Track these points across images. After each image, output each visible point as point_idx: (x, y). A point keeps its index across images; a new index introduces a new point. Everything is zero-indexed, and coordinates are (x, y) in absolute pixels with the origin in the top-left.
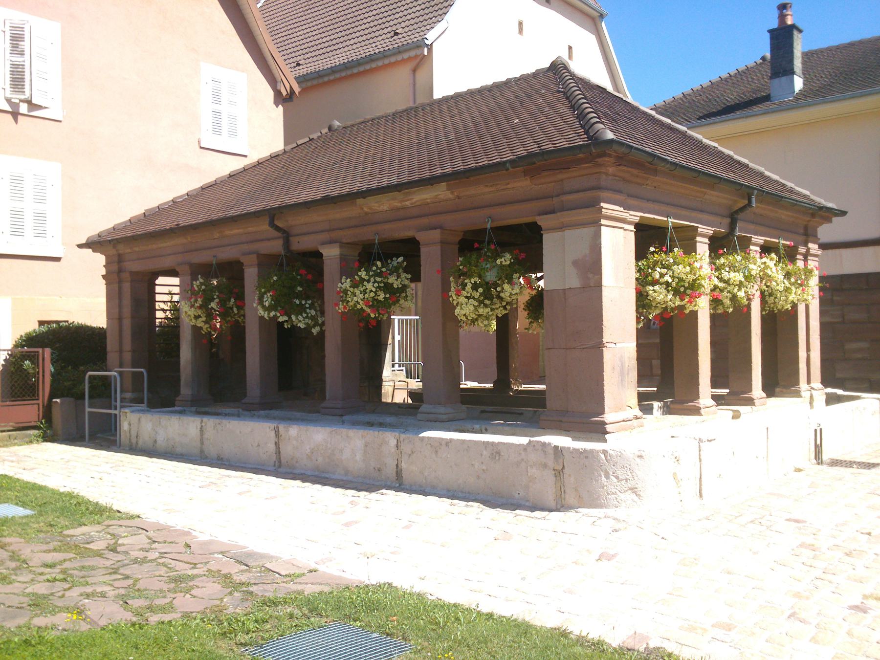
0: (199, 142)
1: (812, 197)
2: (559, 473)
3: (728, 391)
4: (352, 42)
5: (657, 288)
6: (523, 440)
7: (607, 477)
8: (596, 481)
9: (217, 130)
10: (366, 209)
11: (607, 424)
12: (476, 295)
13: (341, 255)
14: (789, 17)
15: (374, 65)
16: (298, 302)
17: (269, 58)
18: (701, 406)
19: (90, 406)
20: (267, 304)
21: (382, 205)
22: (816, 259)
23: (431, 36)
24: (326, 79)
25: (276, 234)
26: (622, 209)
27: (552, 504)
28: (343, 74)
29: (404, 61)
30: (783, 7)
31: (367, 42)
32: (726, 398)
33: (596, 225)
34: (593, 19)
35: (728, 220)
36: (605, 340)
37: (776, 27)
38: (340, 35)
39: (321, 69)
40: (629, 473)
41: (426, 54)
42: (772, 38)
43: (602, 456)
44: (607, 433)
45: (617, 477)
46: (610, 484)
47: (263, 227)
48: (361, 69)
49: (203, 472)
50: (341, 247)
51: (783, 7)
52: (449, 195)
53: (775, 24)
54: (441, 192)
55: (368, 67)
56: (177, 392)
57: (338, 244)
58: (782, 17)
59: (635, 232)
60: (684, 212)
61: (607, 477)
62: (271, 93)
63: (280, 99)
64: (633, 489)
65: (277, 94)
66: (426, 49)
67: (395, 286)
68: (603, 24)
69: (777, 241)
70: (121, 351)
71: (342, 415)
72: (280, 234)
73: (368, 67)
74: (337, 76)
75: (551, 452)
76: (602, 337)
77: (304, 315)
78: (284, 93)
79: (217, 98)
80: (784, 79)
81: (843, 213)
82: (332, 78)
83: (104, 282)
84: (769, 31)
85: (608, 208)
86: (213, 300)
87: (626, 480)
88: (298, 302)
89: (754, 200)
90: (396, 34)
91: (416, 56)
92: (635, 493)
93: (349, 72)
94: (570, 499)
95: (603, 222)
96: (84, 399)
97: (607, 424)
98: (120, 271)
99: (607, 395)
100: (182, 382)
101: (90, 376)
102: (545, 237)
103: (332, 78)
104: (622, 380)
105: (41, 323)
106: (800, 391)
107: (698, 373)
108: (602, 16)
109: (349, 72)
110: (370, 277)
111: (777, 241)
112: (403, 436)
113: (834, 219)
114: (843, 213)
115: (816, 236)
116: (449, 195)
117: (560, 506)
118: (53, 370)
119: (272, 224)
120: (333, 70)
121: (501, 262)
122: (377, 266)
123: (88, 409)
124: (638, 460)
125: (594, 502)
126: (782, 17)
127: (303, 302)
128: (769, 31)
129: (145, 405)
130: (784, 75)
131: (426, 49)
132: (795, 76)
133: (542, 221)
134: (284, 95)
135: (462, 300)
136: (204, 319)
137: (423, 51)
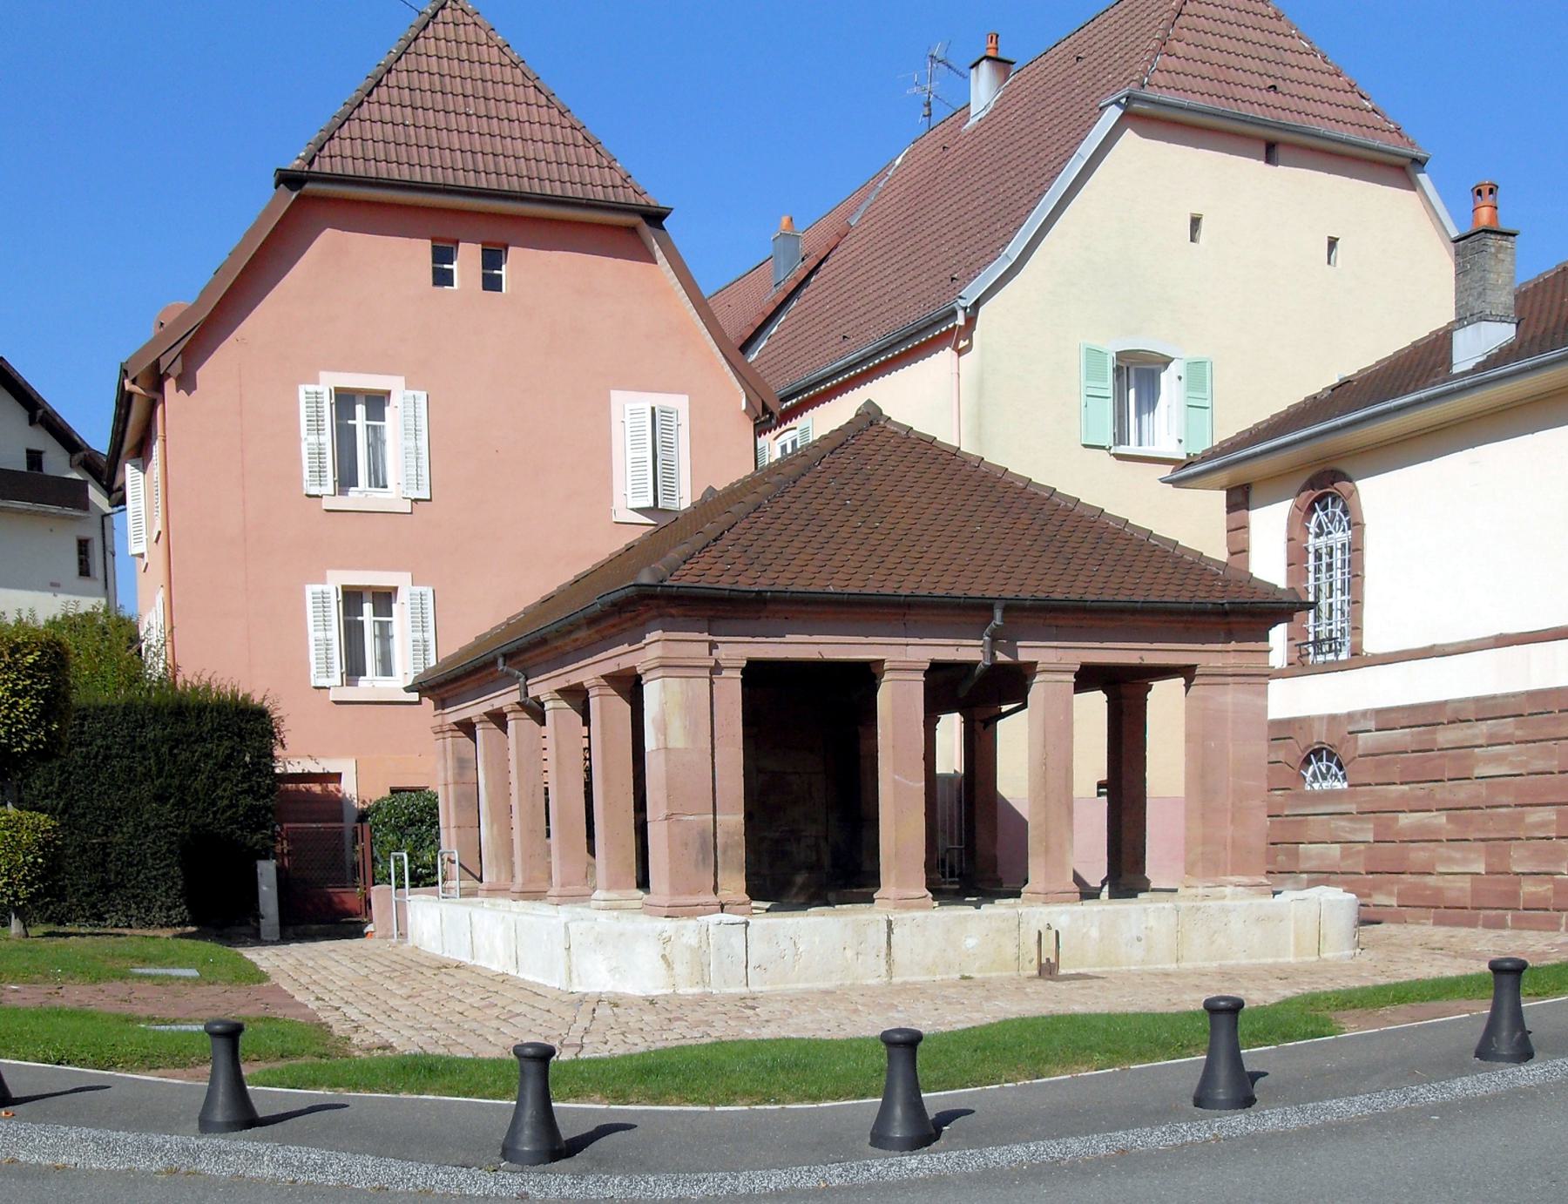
104: (704, 858)
108: (1419, 163)
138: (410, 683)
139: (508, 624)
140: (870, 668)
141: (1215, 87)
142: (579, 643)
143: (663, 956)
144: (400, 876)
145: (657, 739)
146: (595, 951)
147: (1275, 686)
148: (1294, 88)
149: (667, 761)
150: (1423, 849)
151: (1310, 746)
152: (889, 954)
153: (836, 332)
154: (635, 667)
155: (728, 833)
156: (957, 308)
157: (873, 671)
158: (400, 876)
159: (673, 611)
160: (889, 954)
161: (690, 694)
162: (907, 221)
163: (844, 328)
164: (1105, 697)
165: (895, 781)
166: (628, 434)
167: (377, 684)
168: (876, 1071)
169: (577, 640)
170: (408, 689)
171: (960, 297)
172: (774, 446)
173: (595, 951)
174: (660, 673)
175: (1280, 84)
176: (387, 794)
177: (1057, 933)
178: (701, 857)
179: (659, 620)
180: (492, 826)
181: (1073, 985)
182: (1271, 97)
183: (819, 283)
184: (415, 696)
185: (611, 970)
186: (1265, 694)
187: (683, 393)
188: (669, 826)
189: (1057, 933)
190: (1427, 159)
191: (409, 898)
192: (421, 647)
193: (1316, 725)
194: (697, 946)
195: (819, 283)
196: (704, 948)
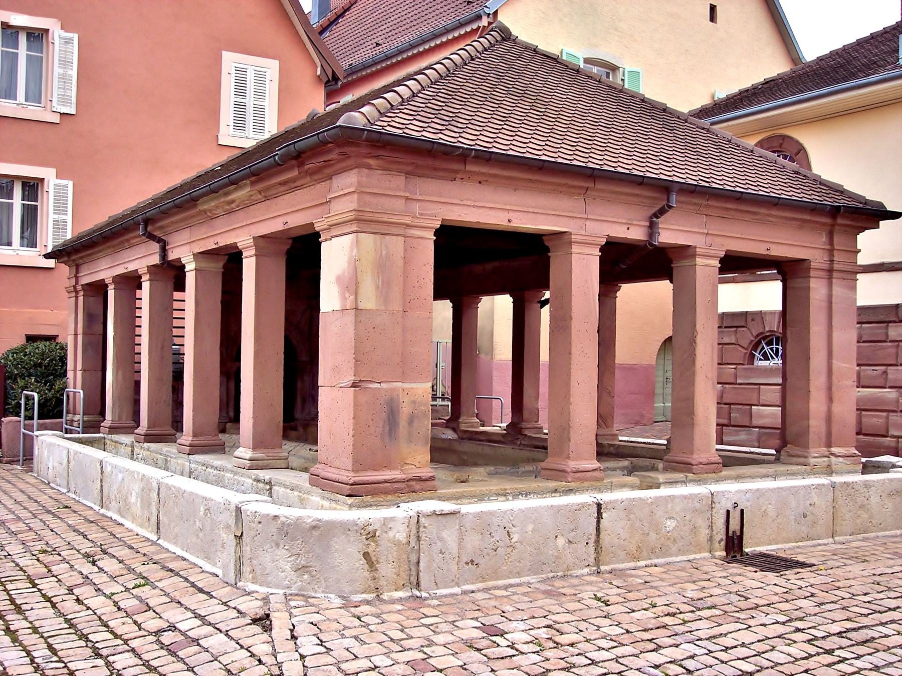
9: (240, 124)
79: (240, 90)
104: (390, 430)
138: (49, 250)
140: (542, 241)
142: (233, 205)
143: (366, 555)
144: (29, 409)
145: (344, 299)
146: (278, 545)
147: (863, 279)
149: (357, 323)
150: (876, 416)
151: (762, 333)
153: (373, 41)
154: (313, 224)
156: (482, 14)
157: (546, 243)
158: (29, 409)
159: (372, 162)
160: (597, 541)
161: (384, 252)
164: (511, 299)
166: (233, 84)
167: (20, 253)
168: (348, 535)
169: (233, 202)
170: (47, 256)
171: (486, 7)
172: (329, 109)
173: (278, 545)
174: (354, 228)
176: (23, 341)
177: (742, 511)
178: (387, 428)
179: (355, 171)
180: (117, 372)
184: (51, 263)
185: (301, 569)
186: (854, 288)
188: (355, 397)
189: (742, 511)
191: (37, 433)
192: (59, 226)
193: (768, 318)
194: (404, 541)
196: (413, 544)
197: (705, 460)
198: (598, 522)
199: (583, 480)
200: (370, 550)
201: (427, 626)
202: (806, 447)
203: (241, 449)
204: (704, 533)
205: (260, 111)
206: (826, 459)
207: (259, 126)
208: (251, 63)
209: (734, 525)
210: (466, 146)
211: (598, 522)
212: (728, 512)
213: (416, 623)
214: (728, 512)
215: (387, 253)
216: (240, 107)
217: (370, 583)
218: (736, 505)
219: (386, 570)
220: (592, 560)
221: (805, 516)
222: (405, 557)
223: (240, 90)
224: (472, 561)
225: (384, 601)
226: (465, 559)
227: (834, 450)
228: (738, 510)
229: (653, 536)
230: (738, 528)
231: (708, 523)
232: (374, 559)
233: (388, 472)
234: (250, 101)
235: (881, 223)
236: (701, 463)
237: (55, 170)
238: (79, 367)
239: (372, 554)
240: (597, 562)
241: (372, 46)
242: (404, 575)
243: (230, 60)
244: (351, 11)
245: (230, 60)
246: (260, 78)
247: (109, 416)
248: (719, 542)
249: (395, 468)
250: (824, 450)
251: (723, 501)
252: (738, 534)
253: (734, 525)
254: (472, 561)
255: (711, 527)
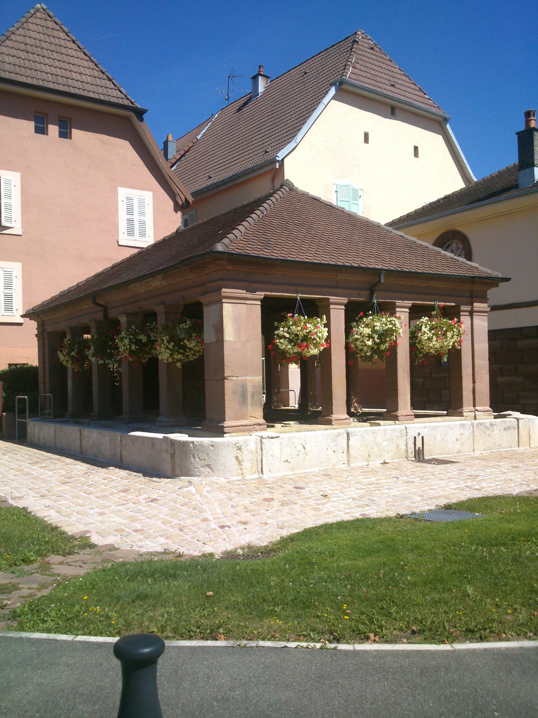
0: (118, 242)
1: (481, 268)
2: (173, 455)
3: (386, 410)
4: (244, 158)
5: (282, 341)
6: (160, 436)
7: (194, 458)
8: (189, 460)
9: (131, 232)
10: (135, 292)
11: (224, 427)
12: (171, 346)
13: (127, 321)
14: (533, 121)
15: (248, 177)
16: (109, 351)
17: (169, 180)
18: (333, 419)
19: (18, 418)
20: (65, 353)
21: (139, 289)
22: (486, 314)
23: (280, 155)
24: (221, 188)
25: (99, 308)
26: (244, 292)
27: (170, 476)
28: (231, 184)
29: (266, 173)
30: (528, 114)
31: (246, 161)
32: (384, 415)
33: (220, 302)
34: (439, 123)
35: (368, 292)
36: (226, 375)
37: (524, 129)
38: (237, 154)
39: (218, 181)
40: (205, 455)
41: (278, 167)
42: (519, 139)
43: (191, 445)
44: (225, 433)
45: (199, 458)
46: (196, 462)
47: (88, 305)
48: (241, 180)
49: (43, 455)
50: (127, 316)
51: (528, 114)
52: (164, 283)
53: (522, 128)
54: (156, 283)
55: (245, 178)
56: (66, 409)
57: (124, 315)
58: (528, 122)
59: (261, 305)
60: (319, 290)
61: (194, 458)
62: (172, 203)
63: (177, 207)
64: (209, 466)
65: (176, 204)
66: (277, 164)
67: (143, 341)
68: (448, 126)
69: (433, 303)
70: (44, 383)
71: (128, 423)
72: (101, 309)
73: (245, 178)
74: (228, 185)
75: (169, 442)
76: (224, 373)
77: (113, 360)
78: (180, 203)
79: (130, 211)
80: (527, 171)
81: (508, 280)
82: (225, 187)
83: (37, 339)
84: (516, 133)
85: (225, 291)
86: (73, 350)
87: (204, 460)
88: (109, 351)
89: (382, 277)
90: (266, 152)
91: (273, 169)
92: (210, 468)
93: (234, 183)
94: (178, 472)
95: (224, 300)
96: (26, 413)
97: (224, 427)
98: (43, 331)
99: (227, 410)
100: (69, 404)
101: (18, 398)
102: (204, 309)
103: (225, 187)
104: (243, 400)
105: (10, 365)
106: (462, 412)
107: (332, 397)
108: (446, 120)
109: (234, 183)
110: (127, 335)
111: (433, 303)
112: (123, 434)
113: (500, 284)
114: (508, 280)
115: (486, 298)
116: (164, 283)
117: (173, 475)
118: (4, 395)
119: (94, 302)
120: (224, 182)
121: (183, 326)
122: (132, 328)
123: (17, 420)
124: (211, 448)
125: (188, 474)
126: (528, 122)
127: (113, 351)
128: (516, 133)
129: (51, 417)
130: (527, 168)
131: (277, 164)
132: (535, 168)
133: (203, 300)
134: (180, 204)
135: (163, 350)
136: (71, 362)
137: (276, 166)
139: (423, 208)
141: (373, 82)
143: (237, 458)
148: (400, 87)
152: (348, 451)
153: (207, 175)
155: (254, 386)
160: (348, 451)
162: (228, 136)
163: (211, 173)
165: (63, 335)
170: (22, 316)
175: (396, 85)
177: (423, 437)
178: (242, 399)
181: (302, 428)
182: (392, 89)
183: (185, 161)
187: (149, 190)
189: (423, 437)
190: (450, 119)
195: (185, 161)
197: (405, 414)
198: (348, 442)
199: (340, 424)
200: (238, 455)
201: (269, 488)
202: (461, 406)
203: (160, 417)
204: (403, 448)
205: (142, 224)
206: (473, 413)
207: (143, 234)
208: (136, 194)
209: (419, 444)
210: (274, 257)
211: (348, 442)
212: (415, 437)
213: (263, 487)
214: (415, 437)
215: (238, 313)
216: (130, 222)
217: (240, 471)
218: (419, 434)
219: (246, 465)
220: (346, 462)
221: (457, 440)
222: (255, 458)
223: (130, 211)
224: (287, 461)
225: (246, 480)
226: (283, 460)
227: (477, 408)
228: (420, 436)
229: (376, 449)
230: (421, 446)
231: (405, 443)
232: (240, 459)
233: (243, 421)
234: (136, 217)
235: (500, 284)
236: (403, 415)
237: (21, 264)
238: (47, 381)
239: (240, 457)
240: (348, 461)
241: (206, 178)
242: (255, 467)
243: (123, 193)
244: (190, 152)
245: (123, 193)
246: (142, 203)
247: (70, 408)
248: (411, 453)
249: (247, 419)
250: (472, 408)
251: (412, 432)
252: (421, 449)
253: (419, 444)
254: (287, 461)
255: (407, 445)
